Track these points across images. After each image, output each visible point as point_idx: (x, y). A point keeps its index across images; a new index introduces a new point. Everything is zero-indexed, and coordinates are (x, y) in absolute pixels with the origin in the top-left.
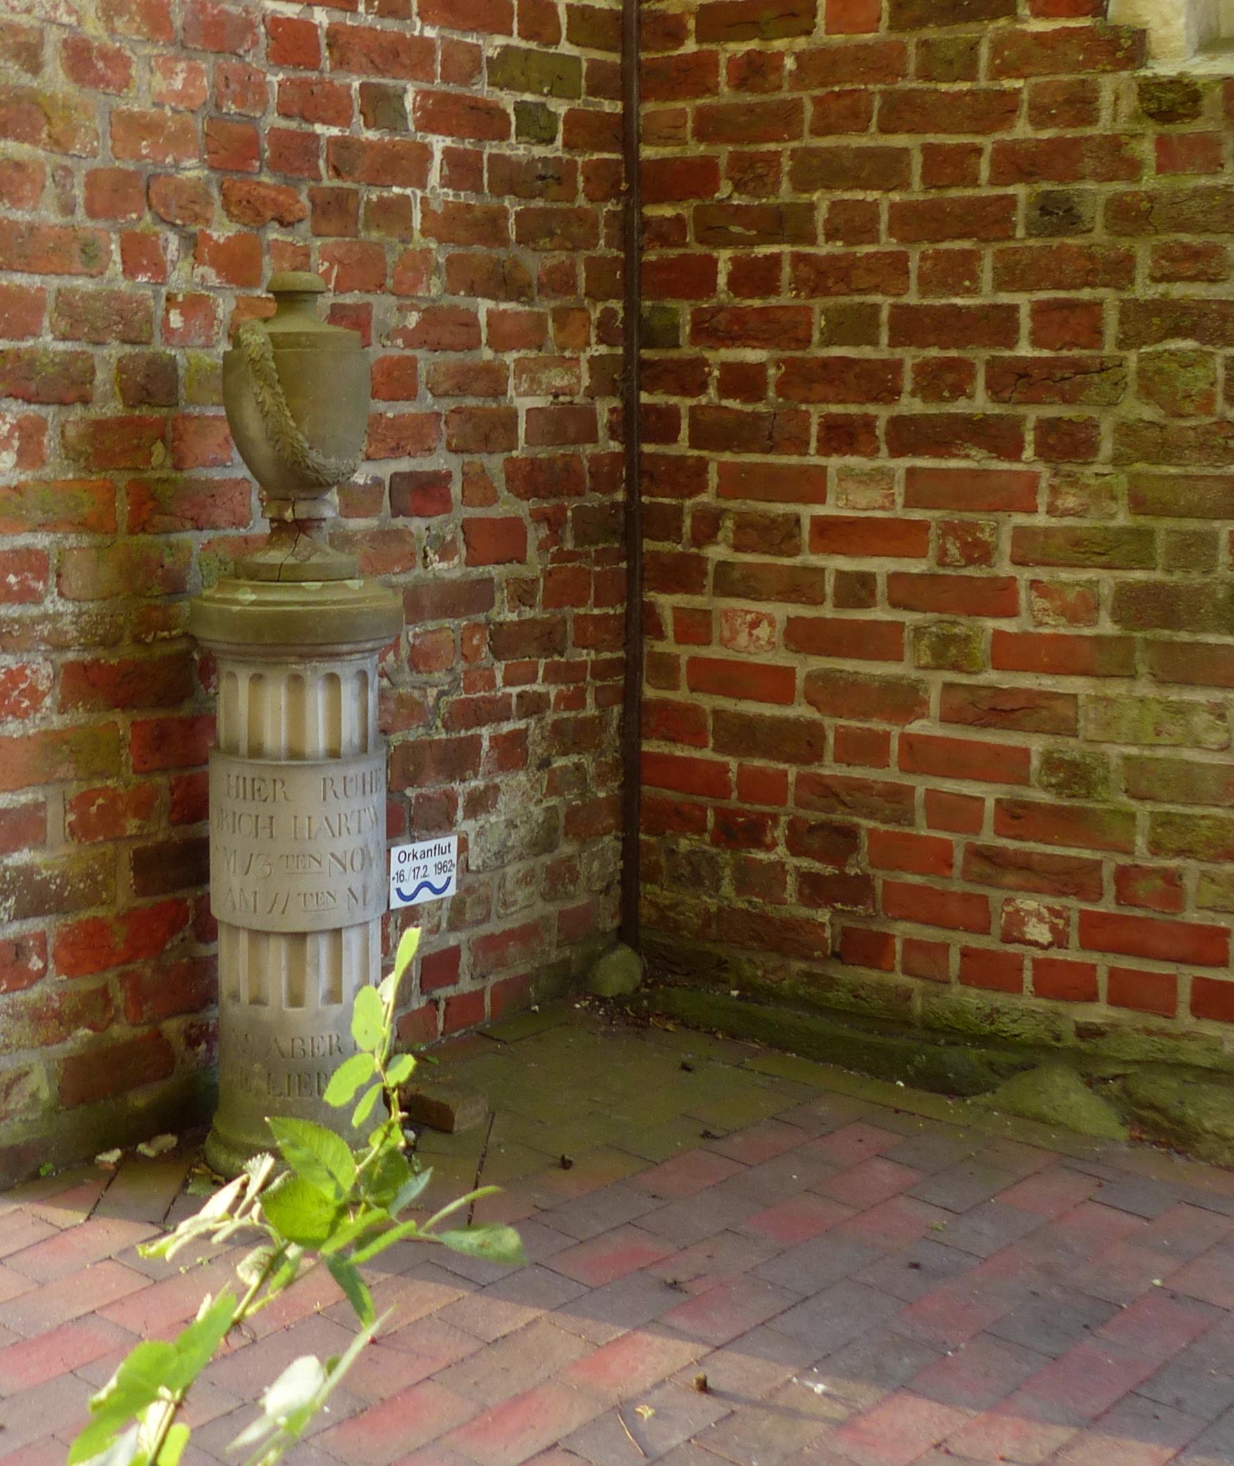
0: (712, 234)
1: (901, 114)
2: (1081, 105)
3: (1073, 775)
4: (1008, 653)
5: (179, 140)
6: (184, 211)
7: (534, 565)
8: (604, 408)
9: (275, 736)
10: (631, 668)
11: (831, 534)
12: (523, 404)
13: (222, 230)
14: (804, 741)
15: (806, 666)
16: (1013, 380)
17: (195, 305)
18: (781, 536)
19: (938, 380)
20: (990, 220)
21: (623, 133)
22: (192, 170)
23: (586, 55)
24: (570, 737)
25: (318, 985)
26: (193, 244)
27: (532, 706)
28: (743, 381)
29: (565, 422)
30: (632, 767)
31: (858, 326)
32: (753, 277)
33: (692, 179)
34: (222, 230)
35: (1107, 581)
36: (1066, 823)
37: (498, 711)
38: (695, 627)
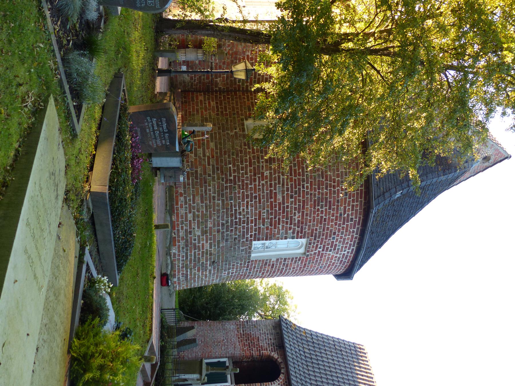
0: (231, 96)
1: (241, 106)
2: (242, 115)
3: (194, 115)
4: (202, 112)
5: (236, 49)
6: (232, 49)
7: (206, 81)
8: (217, 89)
9: (198, 52)
10: (197, 92)
11: (209, 103)
12: (218, 80)
13: (231, 52)
14: (193, 100)
15: (199, 101)
16: (222, 112)
17: (225, 50)
18: (209, 99)
19: (222, 108)
20: (233, 110)
21: (239, 90)
22: (235, 50)
23: (245, 86)
24: (192, 84)
25: (182, 54)
26: (230, 50)
27: (195, 81)
28: (220, 98)
29: (217, 84)
30: (189, 91)
31: (225, 103)
32: (228, 98)
33: (236, 94)
34: (231, 52)
35: (208, 117)
36: (190, 114)
37: (195, 77)
38: (201, 95)
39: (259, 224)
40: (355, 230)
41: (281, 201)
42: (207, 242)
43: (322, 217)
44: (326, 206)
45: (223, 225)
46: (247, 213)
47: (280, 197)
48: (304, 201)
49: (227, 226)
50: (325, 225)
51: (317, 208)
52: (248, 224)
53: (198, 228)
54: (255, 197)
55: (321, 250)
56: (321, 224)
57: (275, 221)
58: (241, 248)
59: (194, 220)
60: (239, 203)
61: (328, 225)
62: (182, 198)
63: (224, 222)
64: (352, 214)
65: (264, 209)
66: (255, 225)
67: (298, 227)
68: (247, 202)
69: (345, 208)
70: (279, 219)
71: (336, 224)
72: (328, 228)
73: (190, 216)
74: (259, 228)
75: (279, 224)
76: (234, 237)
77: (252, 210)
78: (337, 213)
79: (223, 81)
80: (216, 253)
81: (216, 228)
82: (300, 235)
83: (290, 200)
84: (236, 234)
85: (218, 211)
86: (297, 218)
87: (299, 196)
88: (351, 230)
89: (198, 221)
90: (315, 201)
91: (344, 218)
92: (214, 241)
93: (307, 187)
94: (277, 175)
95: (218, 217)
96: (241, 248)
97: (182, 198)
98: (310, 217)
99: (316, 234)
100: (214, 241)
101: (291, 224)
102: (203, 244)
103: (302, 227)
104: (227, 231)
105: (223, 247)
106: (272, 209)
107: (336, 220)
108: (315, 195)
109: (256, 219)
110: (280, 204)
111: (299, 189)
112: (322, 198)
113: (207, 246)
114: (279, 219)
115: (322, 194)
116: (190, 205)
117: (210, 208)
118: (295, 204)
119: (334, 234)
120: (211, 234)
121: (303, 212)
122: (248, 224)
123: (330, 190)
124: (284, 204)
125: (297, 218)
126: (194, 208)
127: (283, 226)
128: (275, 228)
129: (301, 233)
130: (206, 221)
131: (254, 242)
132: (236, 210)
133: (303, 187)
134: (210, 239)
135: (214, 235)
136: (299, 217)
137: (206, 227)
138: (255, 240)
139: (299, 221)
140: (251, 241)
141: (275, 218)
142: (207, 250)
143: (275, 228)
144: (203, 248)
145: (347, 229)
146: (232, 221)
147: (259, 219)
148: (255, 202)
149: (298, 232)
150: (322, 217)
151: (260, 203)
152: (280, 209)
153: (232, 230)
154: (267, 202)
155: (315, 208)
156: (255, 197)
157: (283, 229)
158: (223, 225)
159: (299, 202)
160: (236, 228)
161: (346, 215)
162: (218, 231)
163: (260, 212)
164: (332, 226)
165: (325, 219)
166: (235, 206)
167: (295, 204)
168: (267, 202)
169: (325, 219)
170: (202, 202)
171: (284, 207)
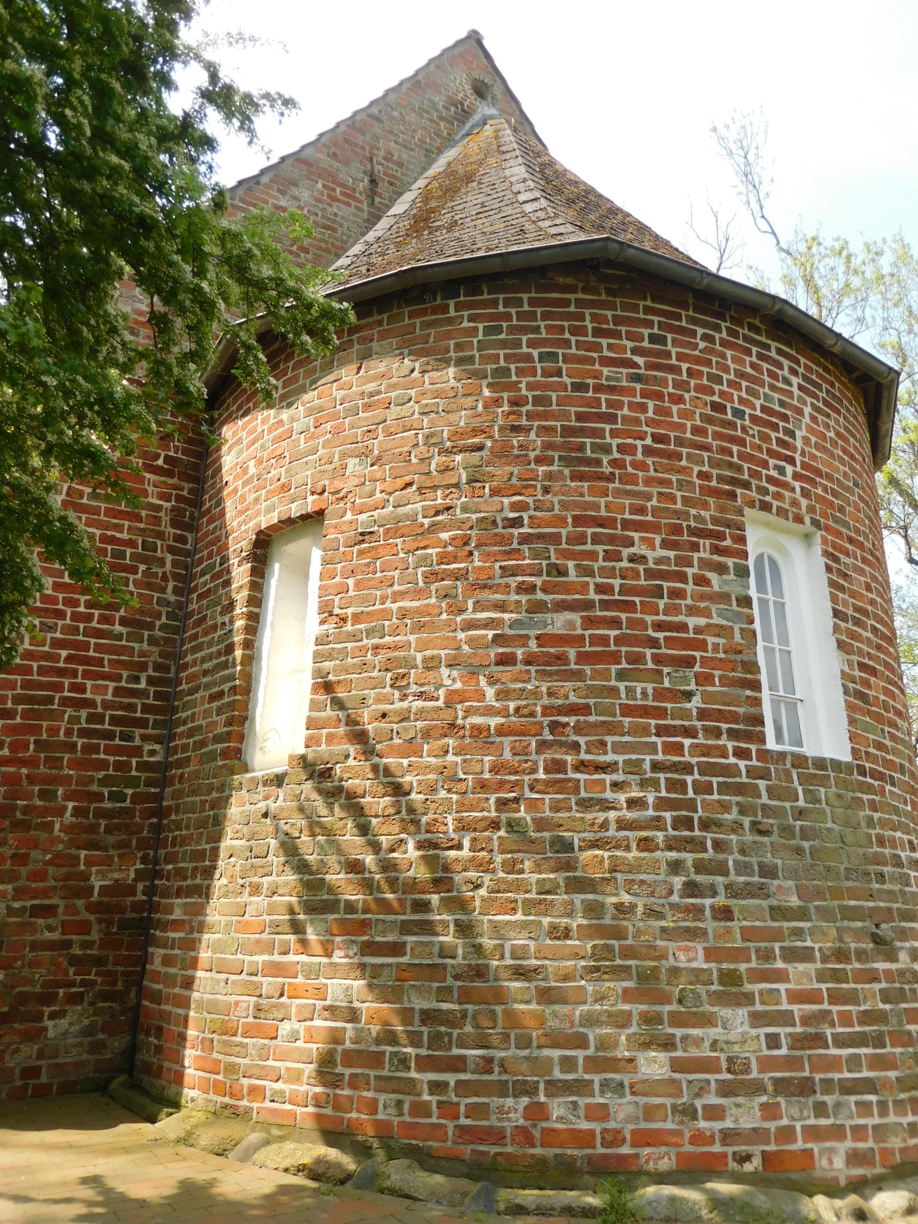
7: (95, 936)
39: (686, 714)
42: (780, 976)
44: (599, 433)
46: (633, 767)
52: (687, 769)
62: (558, 1108)
65: (614, 692)
66: (689, 732)
67: (695, 547)
68: (581, 766)
69: (606, 362)
72: (696, 430)
74: (703, 714)
75: (683, 627)
77: (619, 748)
79: (108, 862)
81: (710, 925)
89: (677, 1020)
92: (777, 935)
96: (801, 803)
97: (558, 1108)
103: (693, 532)
106: (614, 658)
107: (659, 396)
109: (661, 731)
113: (801, 974)
114: (659, 626)
122: (687, 769)
124: (588, 605)
127: (693, 611)
134: (767, 956)
135: (748, 934)
139: (665, 545)
140: (764, 755)
141: (654, 643)
152: (615, 623)
157: (707, 613)
158: (692, 889)
159: (581, 539)
163: (627, 711)
165: (657, 438)
169: (657, 438)
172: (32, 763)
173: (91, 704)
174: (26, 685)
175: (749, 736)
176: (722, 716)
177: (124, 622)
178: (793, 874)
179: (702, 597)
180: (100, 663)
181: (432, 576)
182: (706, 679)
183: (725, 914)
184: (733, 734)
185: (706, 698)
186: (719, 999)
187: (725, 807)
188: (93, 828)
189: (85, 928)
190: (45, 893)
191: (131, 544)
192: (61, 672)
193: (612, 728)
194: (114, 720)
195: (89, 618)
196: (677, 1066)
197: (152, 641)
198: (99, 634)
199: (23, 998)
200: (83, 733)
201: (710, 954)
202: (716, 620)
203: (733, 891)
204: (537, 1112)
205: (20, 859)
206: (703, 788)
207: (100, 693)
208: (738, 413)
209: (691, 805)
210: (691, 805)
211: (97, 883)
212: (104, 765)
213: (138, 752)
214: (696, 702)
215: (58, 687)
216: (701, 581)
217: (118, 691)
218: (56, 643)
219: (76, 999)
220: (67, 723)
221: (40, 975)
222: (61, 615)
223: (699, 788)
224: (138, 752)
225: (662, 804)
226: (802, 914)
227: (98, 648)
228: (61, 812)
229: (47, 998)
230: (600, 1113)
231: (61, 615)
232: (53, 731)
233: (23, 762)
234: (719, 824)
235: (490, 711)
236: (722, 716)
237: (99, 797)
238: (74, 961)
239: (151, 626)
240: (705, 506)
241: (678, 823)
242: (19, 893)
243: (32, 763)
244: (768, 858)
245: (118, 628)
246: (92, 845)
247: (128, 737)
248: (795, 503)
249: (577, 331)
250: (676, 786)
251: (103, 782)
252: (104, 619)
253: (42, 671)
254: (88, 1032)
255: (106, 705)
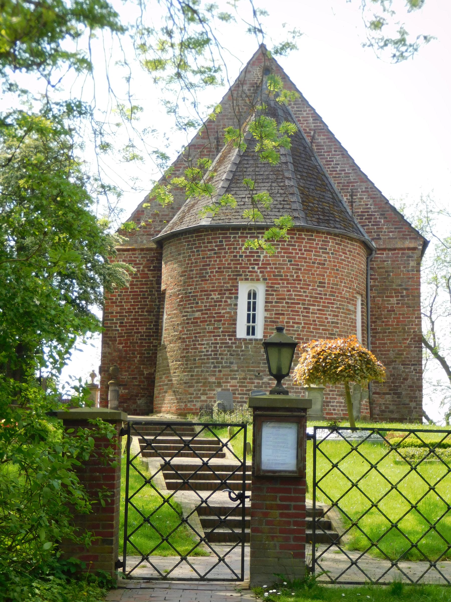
7: (146, 383)
39: (218, 332)
40: (232, 236)
41: (200, 313)
42: (229, 382)
43: (217, 272)
44: (206, 269)
45: (215, 367)
46: (208, 344)
47: (197, 314)
48: (201, 291)
49: (217, 363)
50: (224, 268)
51: (207, 278)
52: (218, 343)
53: (214, 390)
54: (196, 337)
55: (256, 267)
56: (223, 272)
57: (218, 317)
58: (243, 348)
59: (206, 394)
60: (199, 352)
61: (225, 264)
62: (189, 405)
63: (212, 366)
64: (215, 242)
65: (206, 329)
66: (219, 336)
67: (225, 294)
68: (199, 344)
69: (209, 250)
70: (216, 313)
71: (224, 257)
72: (228, 264)
73: (203, 398)
74: (222, 332)
75: (220, 313)
76: (229, 356)
77: (206, 340)
78: (214, 257)
79: (147, 368)
80: (243, 374)
81: (217, 374)
82: (234, 291)
83: (200, 304)
84: (227, 354)
85: (202, 371)
86: (215, 296)
87: (197, 296)
88: (232, 240)
89: (209, 390)
90: (202, 281)
91: (218, 249)
92: (230, 375)
93: (191, 289)
94: (310, 315)
95: (207, 372)
96: (243, 348)
97: (189, 405)
98: (215, 283)
99: (234, 275)
100: (230, 375)
101: (221, 301)
102: (231, 386)
103: (225, 290)
104: (221, 363)
105: (238, 367)
106: (206, 321)
107: (220, 257)
108: (197, 281)
109: (214, 336)
110: (202, 314)
111: (192, 296)
112: (200, 273)
113: (233, 382)
114: (216, 313)
115: (197, 274)
116: (195, 398)
117: (199, 379)
118: (203, 299)
119: (235, 256)
120: (222, 379)
121: (211, 291)
122: (218, 343)
123: (320, 248)
124: (202, 310)
125: (215, 296)
126: (197, 394)
127: (223, 309)
128: (224, 317)
129: (232, 290)
130: (209, 382)
131: (238, 336)
132: (205, 355)
133: (190, 293)
134: (227, 379)
135: (224, 375)
136: (215, 295)
137: (214, 383)
138: (235, 336)
139: (219, 294)
140: (236, 339)
141: (214, 317)
142: (238, 383)
143: (224, 317)
144: (235, 386)
145: (231, 245)
146: (213, 359)
147: (214, 332)
148: (199, 337)
149: (230, 294)
150: (217, 272)
151: (200, 333)
152: (207, 314)
153: (222, 359)
154: (200, 326)
155: (208, 280)
156: (196, 337)
157: (226, 309)
158: (215, 367)
159: (201, 295)
160: (220, 355)
161: (303, 236)
162: (220, 371)
163: (208, 332)
164: (226, 260)
165: (219, 268)
166: (201, 356)
167: (203, 299)
168: (200, 326)
169: (219, 268)
170: (193, 386)
171: (206, 310)
172: (129, 347)
173: (140, 332)
174: (127, 329)
175: (232, 336)
176: (226, 332)
177: (147, 312)
178: (237, 363)
179: (225, 305)
180: (141, 322)
181: (179, 305)
182: (224, 324)
183: (220, 371)
184: (229, 335)
185: (224, 328)
186: (216, 386)
187: (225, 351)
188: (143, 361)
189: (143, 382)
190: (135, 375)
191: (146, 291)
192: (133, 326)
193: (204, 336)
194: (146, 336)
195: (138, 312)
196: (207, 398)
197: (154, 315)
198: (141, 315)
199: (132, 396)
200: (140, 339)
201: (216, 379)
202: (228, 310)
203: (223, 367)
204: (186, 405)
205: (129, 368)
206: (221, 347)
207: (143, 329)
208: (241, 256)
209: (218, 351)
210: (218, 351)
211: (145, 373)
212: (145, 346)
213: (152, 343)
214: (221, 329)
215: (133, 329)
216: (226, 302)
217: (147, 329)
218: (132, 319)
219: (143, 396)
220: (136, 337)
221: (135, 391)
222: (132, 312)
223: (221, 347)
224: (152, 343)
225: (212, 351)
226: (237, 371)
227: (141, 319)
228: (136, 357)
229: (137, 396)
230: (195, 405)
231: (132, 312)
232: (133, 339)
233: (127, 347)
234: (222, 354)
235: (185, 334)
236: (226, 332)
237: (144, 354)
238: (142, 389)
239: (153, 312)
240: (228, 283)
241: (215, 355)
242: (129, 375)
243: (129, 347)
244: (232, 360)
245: (145, 313)
246: (143, 364)
247: (149, 339)
248: (258, 276)
249: (204, 243)
250: (215, 347)
251: (145, 350)
252: (142, 312)
253: (130, 326)
254: (146, 403)
255: (144, 332)
